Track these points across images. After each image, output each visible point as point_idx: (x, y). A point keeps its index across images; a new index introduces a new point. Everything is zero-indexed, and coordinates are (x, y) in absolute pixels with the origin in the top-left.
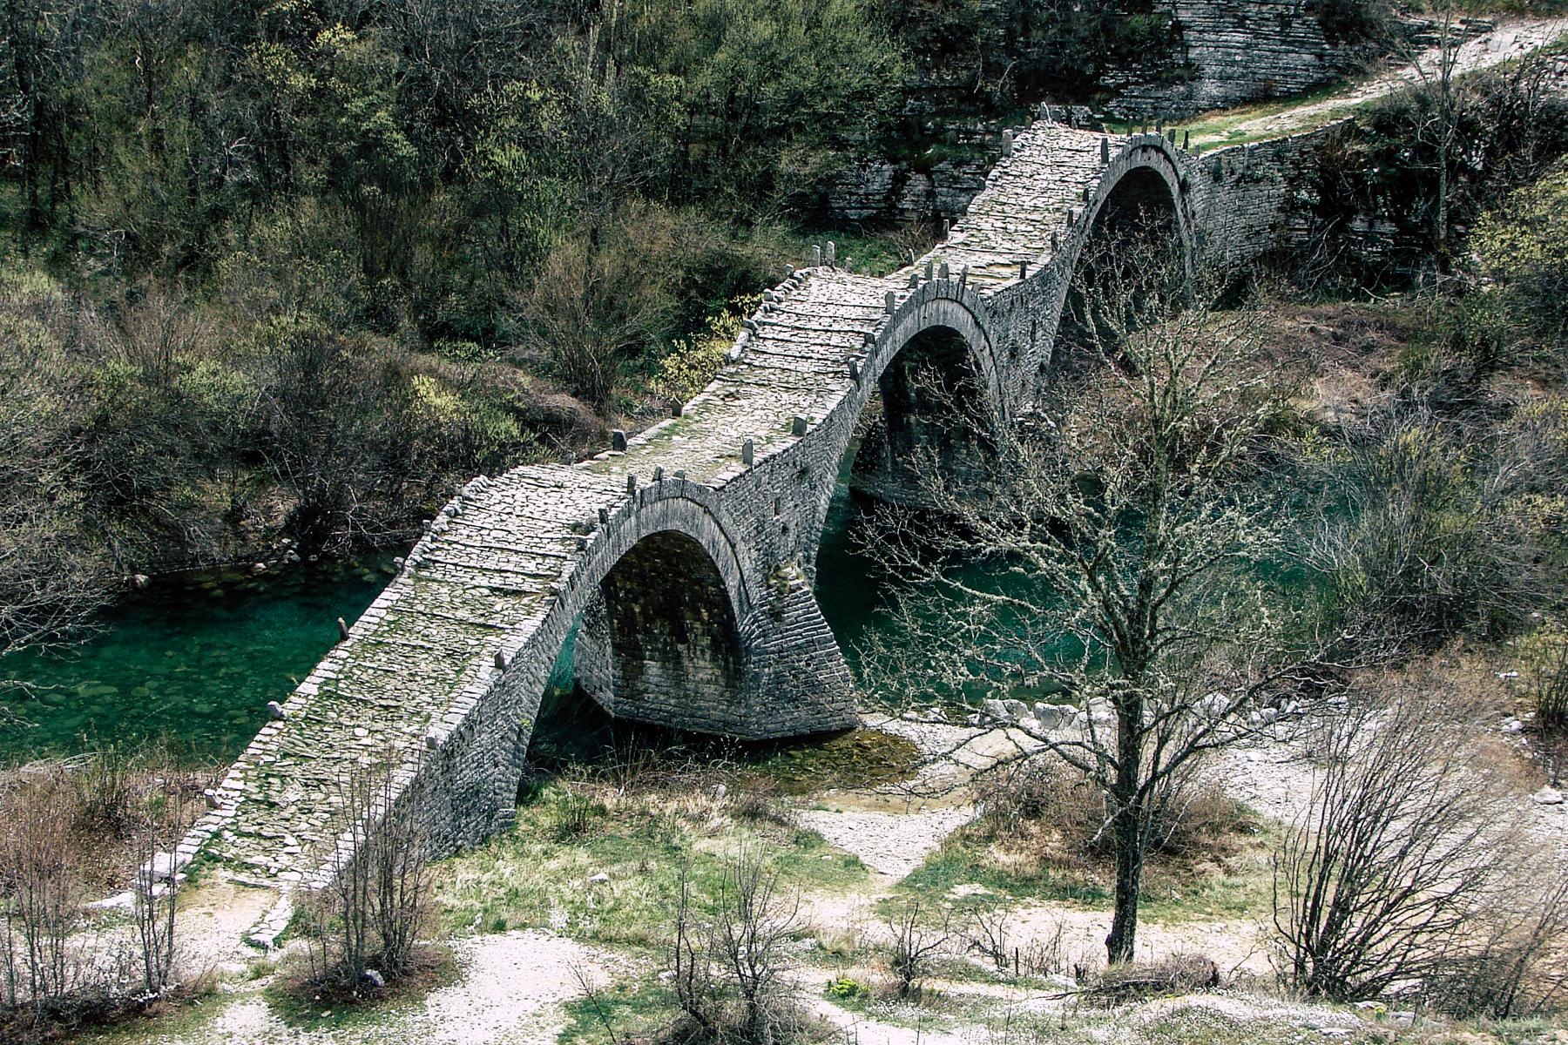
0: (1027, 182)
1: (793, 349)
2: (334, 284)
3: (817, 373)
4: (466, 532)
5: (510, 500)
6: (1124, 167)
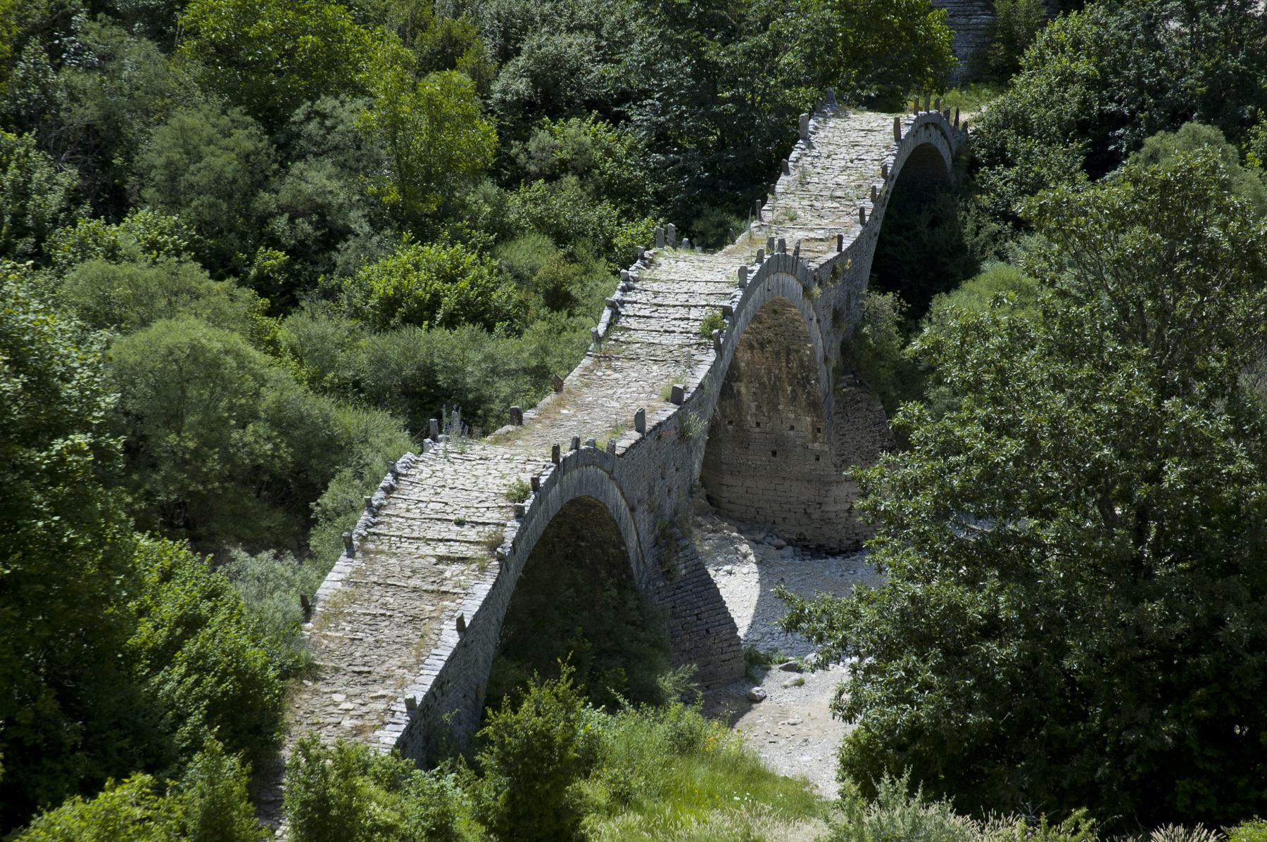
0: (827, 163)
1: (654, 324)
2: (345, 254)
3: (681, 346)
4: (404, 506)
5: (441, 474)
6: (911, 146)
